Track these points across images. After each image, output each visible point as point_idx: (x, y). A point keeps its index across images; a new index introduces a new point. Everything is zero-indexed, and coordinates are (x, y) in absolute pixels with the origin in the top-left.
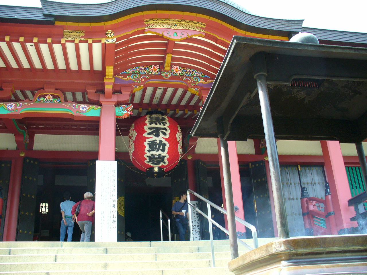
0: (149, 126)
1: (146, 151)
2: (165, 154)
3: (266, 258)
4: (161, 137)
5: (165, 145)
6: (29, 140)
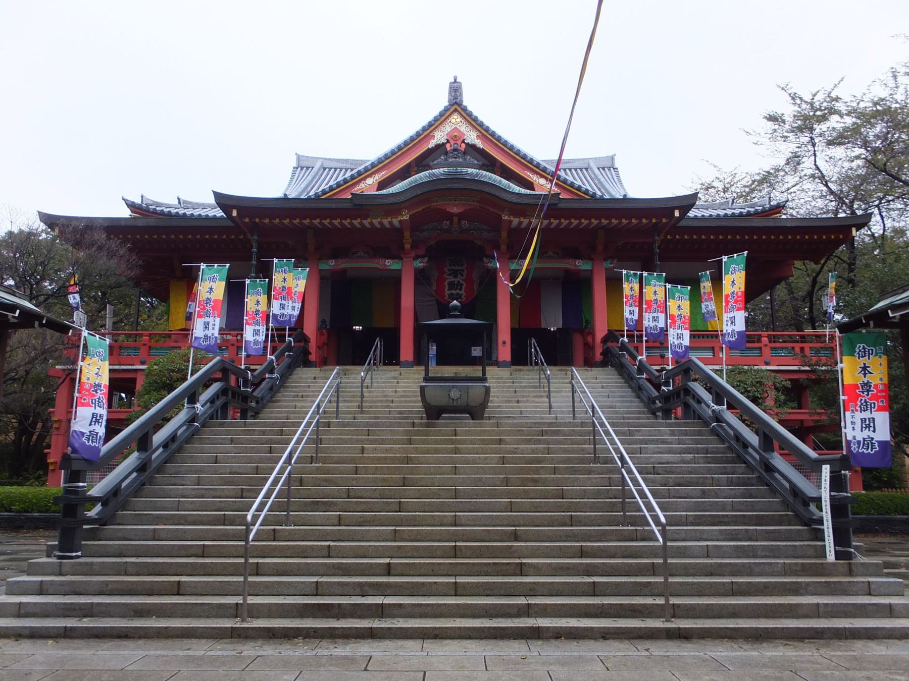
2: (462, 292)
4: (459, 279)
5: (462, 285)
6: (579, 258)
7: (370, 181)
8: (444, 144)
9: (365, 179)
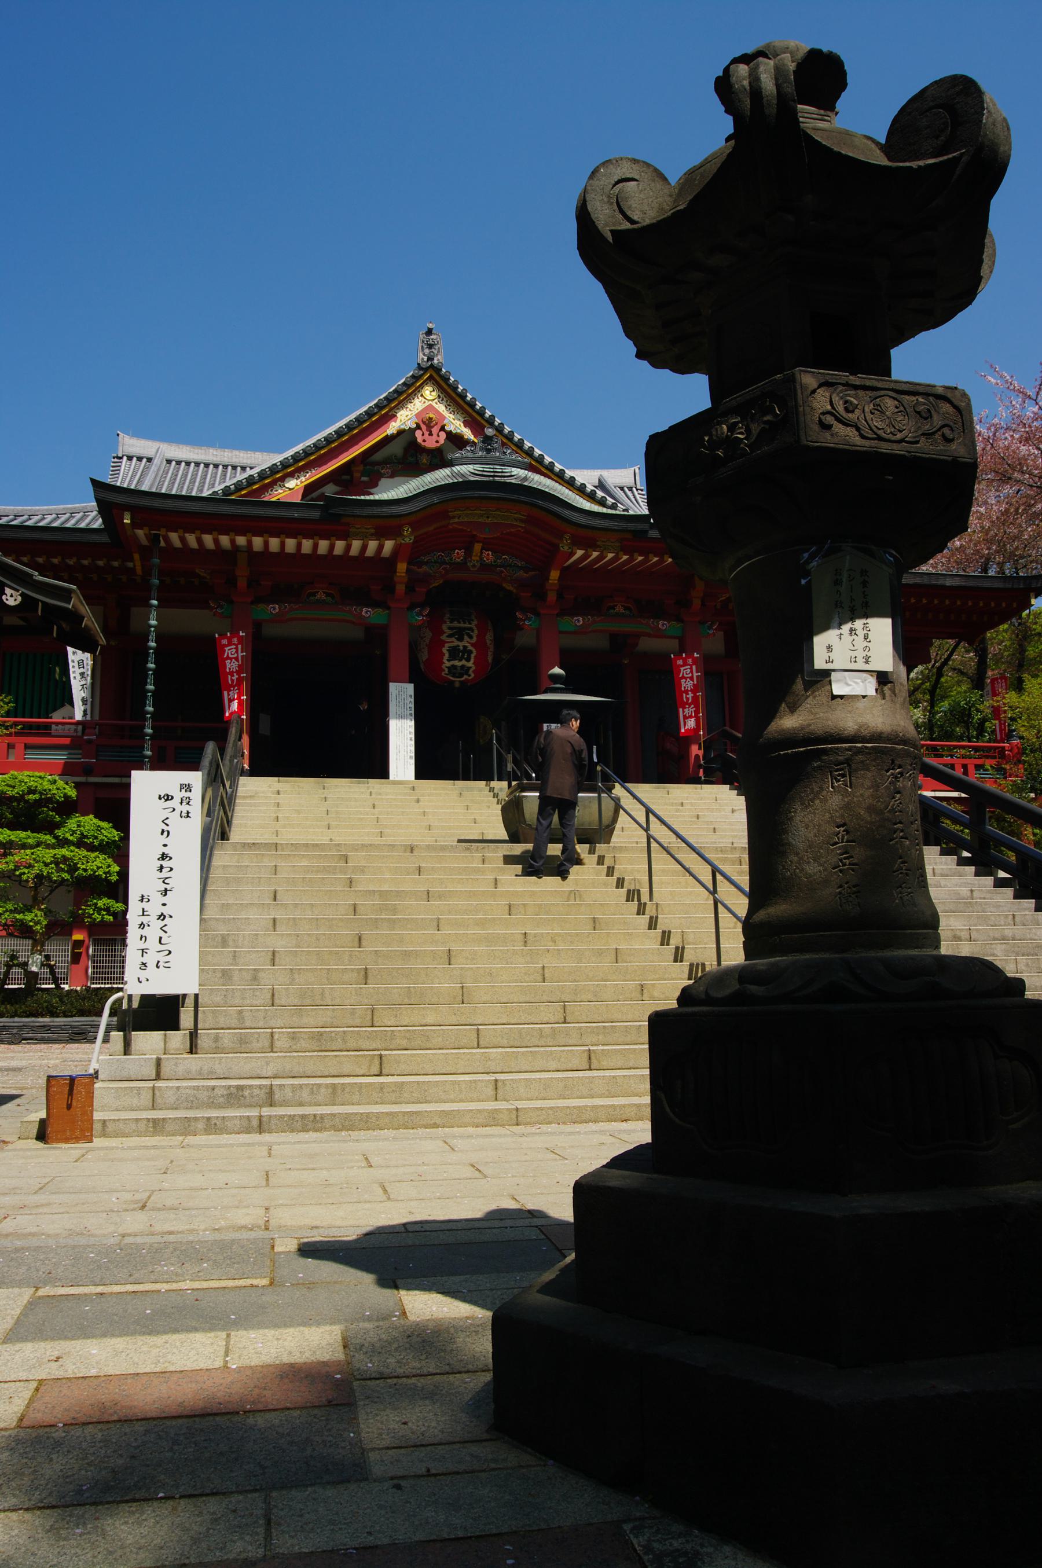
0: (449, 624)
1: (445, 661)
2: (470, 664)
3: (882, 453)
4: (466, 643)
5: (471, 652)
7: (291, 483)
8: (412, 431)
9: (283, 479)
